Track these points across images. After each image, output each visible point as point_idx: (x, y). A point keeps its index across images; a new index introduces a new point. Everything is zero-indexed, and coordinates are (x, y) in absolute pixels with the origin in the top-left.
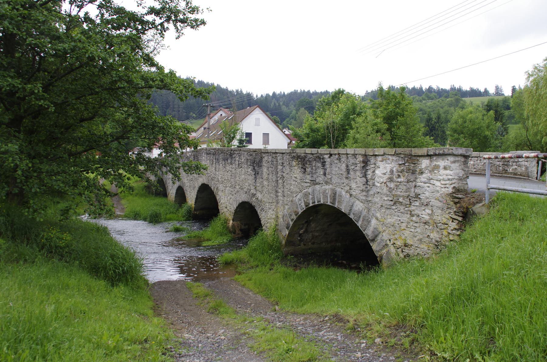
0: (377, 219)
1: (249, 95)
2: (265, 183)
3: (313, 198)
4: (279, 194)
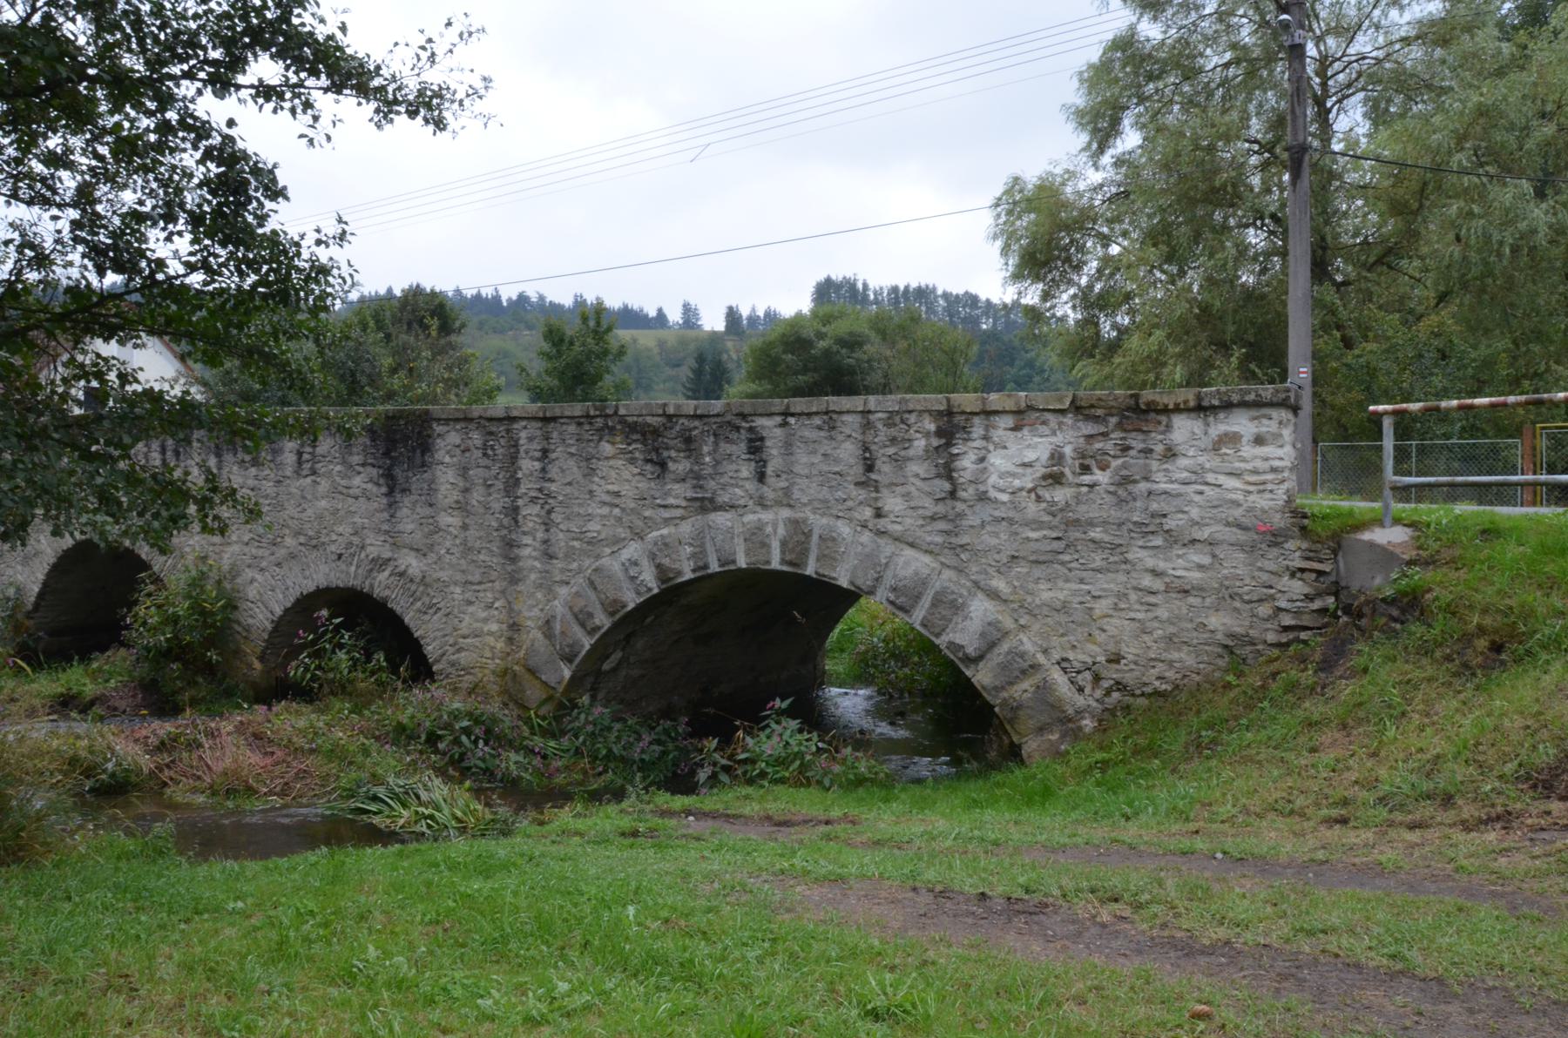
2: (450, 520)
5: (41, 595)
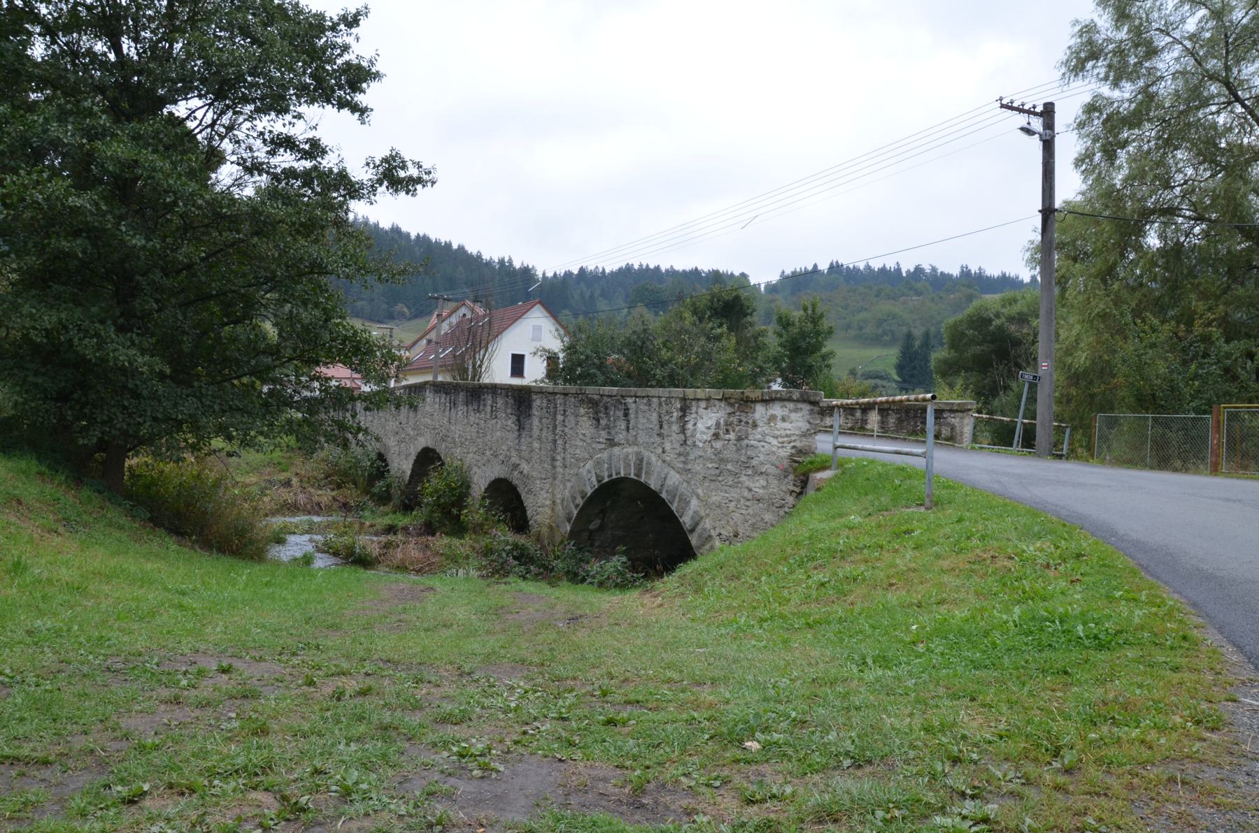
0: (698, 497)
1: (527, 272)
2: (536, 445)
3: (609, 468)
4: (558, 463)
5: (411, 476)
